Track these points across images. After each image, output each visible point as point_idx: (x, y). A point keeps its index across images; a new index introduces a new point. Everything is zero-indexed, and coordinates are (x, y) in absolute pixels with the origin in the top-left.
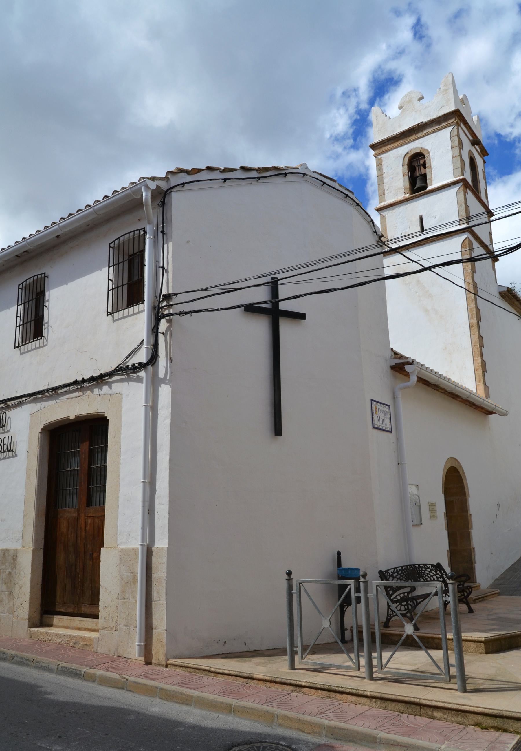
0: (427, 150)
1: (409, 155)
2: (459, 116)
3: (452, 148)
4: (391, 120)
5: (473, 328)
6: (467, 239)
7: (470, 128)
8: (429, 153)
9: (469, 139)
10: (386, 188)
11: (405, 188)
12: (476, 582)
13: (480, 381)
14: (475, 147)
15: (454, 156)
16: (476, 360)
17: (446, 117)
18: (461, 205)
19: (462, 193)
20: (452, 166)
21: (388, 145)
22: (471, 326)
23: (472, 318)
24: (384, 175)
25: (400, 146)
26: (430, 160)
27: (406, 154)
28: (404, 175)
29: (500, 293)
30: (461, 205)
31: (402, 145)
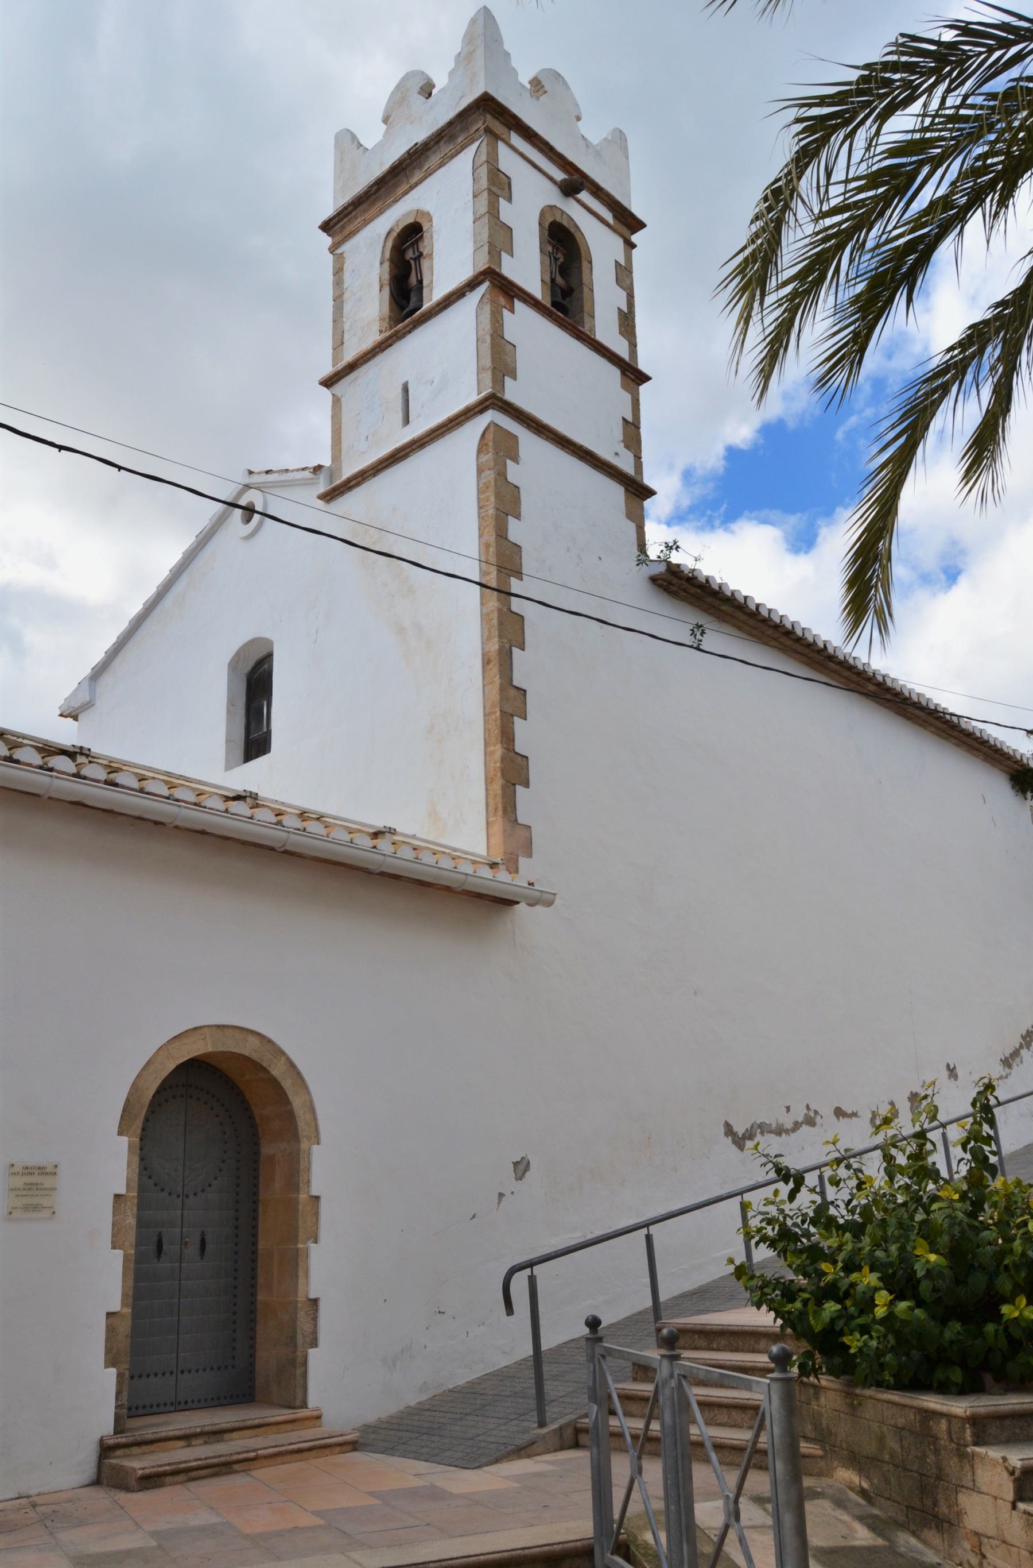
0: (429, 214)
1: (394, 234)
2: (501, 115)
3: (475, 196)
4: (367, 153)
5: (491, 665)
6: (492, 429)
7: (551, 149)
8: (431, 220)
9: (551, 179)
10: (346, 327)
11: (382, 319)
12: (304, 1405)
13: (496, 809)
14: (579, 201)
15: (478, 216)
16: (493, 753)
17: (464, 116)
18: (484, 341)
19: (488, 308)
20: (472, 243)
21: (356, 218)
22: (486, 662)
23: (489, 638)
24: (345, 296)
25: (378, 216)
26: (432, 237)
27: (389, 233)
28: (381, 287)
29: (654, 580)
30: (484, 341)
31: (381, 212)
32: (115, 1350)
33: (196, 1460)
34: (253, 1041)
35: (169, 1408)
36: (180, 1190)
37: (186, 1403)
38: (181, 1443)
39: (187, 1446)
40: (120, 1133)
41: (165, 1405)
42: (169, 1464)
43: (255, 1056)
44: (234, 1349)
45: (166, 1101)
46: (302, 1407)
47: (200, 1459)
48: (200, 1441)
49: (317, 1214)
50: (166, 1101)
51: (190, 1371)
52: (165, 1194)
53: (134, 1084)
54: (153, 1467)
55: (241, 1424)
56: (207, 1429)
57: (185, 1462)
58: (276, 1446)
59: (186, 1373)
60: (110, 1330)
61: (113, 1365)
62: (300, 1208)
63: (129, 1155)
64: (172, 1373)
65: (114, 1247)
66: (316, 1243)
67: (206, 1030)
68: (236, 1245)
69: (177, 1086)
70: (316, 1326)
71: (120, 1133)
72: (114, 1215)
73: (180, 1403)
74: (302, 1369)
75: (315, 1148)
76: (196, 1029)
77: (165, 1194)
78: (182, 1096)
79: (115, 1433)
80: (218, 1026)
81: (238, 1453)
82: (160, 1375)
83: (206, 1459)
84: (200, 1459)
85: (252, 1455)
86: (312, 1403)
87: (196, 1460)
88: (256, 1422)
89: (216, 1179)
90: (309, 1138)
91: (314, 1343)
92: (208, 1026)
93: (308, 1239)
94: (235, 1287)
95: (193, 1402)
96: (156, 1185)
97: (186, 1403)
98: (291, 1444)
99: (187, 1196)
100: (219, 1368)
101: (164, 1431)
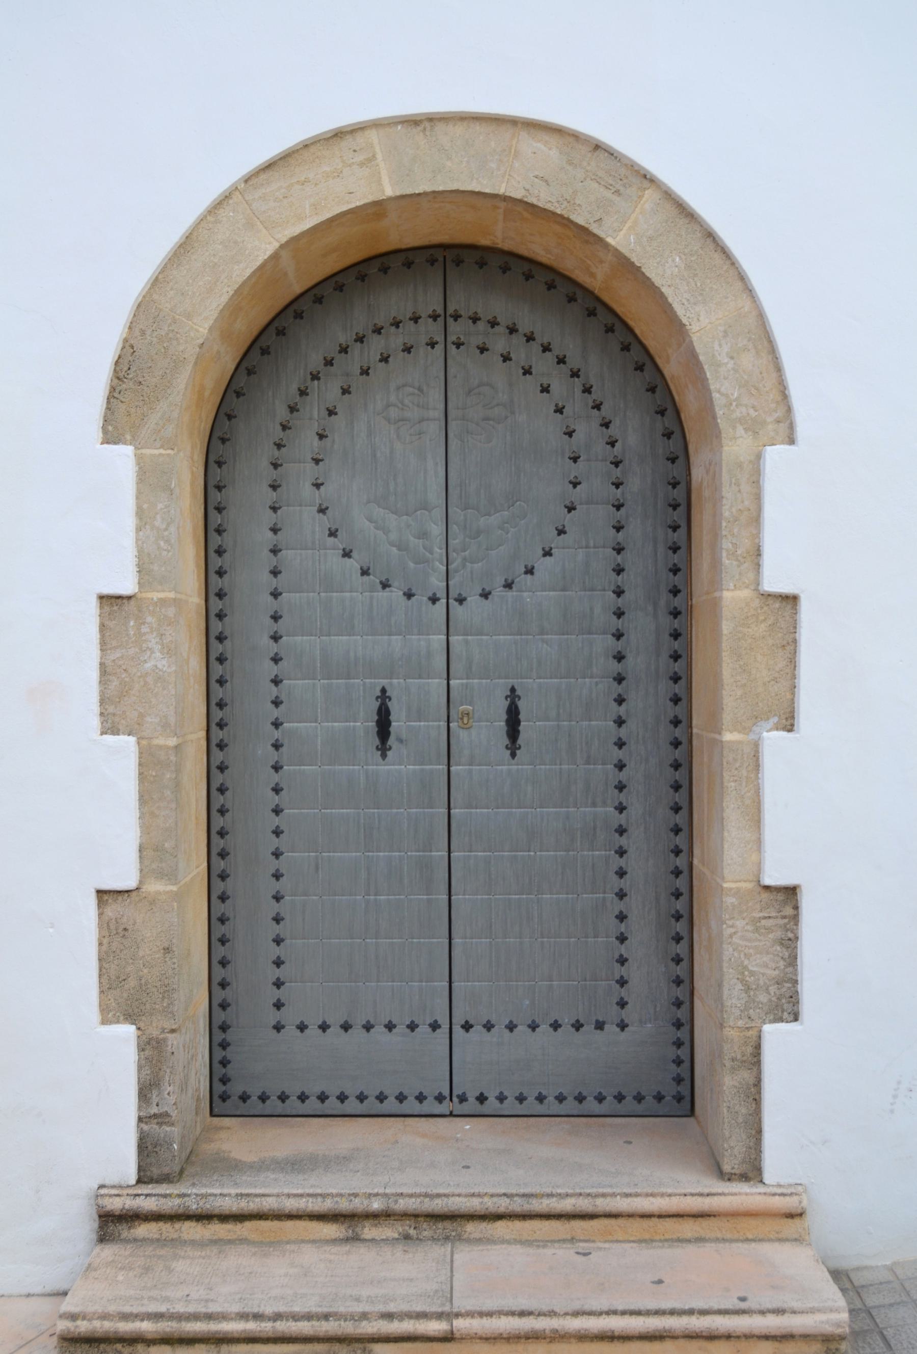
12: (752, 1172)
32: (132, 983)
33: (243, 1316)
34: (542, 153)
35: (430, 1106)
36: (437, 583)
37: (482, 1099)
38: (331, 1230)
39: (347, 1240)
40: (111, 436)
41: (421, 1098)
42: (157, 1317)
43: (543, 197)
44: (622, 982)
45: (385, 359)
46: (744, 1178)
47: (257, 1317)
48: (388, 1231)
49: (790, 646)
50: (385, 359)
51: (489, 1026)
52: (396, 594)
53: (143, 307)
54: (104, 1317)
55: (518, 1205)
56: (402, 1205)
57: (209, 1317)
58: (522, 1314)
59: (478, 1028)
60: (115, 940)
61: (130, 1017)
62: (726, 627)
63: (139, 495)
64: (435, 1026)
65: (110, 727)
66: (790, 728)
67: (373, 136)
68: (620, 722)
69: (416, 319)
70: (792, 960)
71: (111, 436)
72: (104, 646)
73: (463, 1099)
74: (747, 1076)
75: (775, 456)
76: (338, 135)
77: (396, 594)
78: (432, 344)
79: (139, 1181)
80: (413, 122)
81: (389, 1316)
82: (401, 1029)
83: (278, 1317)
84: (257, 1317)
85: (435, 1327)
86: (776, 1167)
87: (243, 1316)
88: (567, 1205)
89: (548, 553)
90: (754, 427)
91: (788, 1007)
92: (376, 124)
93: (757, 718)
94: (621, 831)
95: (501, 1098)
96: (365, 572)
97: (482, 1099)
98: (576, 1314)
99: (461, 600)
100: (578, 1026)
101: (276, 1191)
